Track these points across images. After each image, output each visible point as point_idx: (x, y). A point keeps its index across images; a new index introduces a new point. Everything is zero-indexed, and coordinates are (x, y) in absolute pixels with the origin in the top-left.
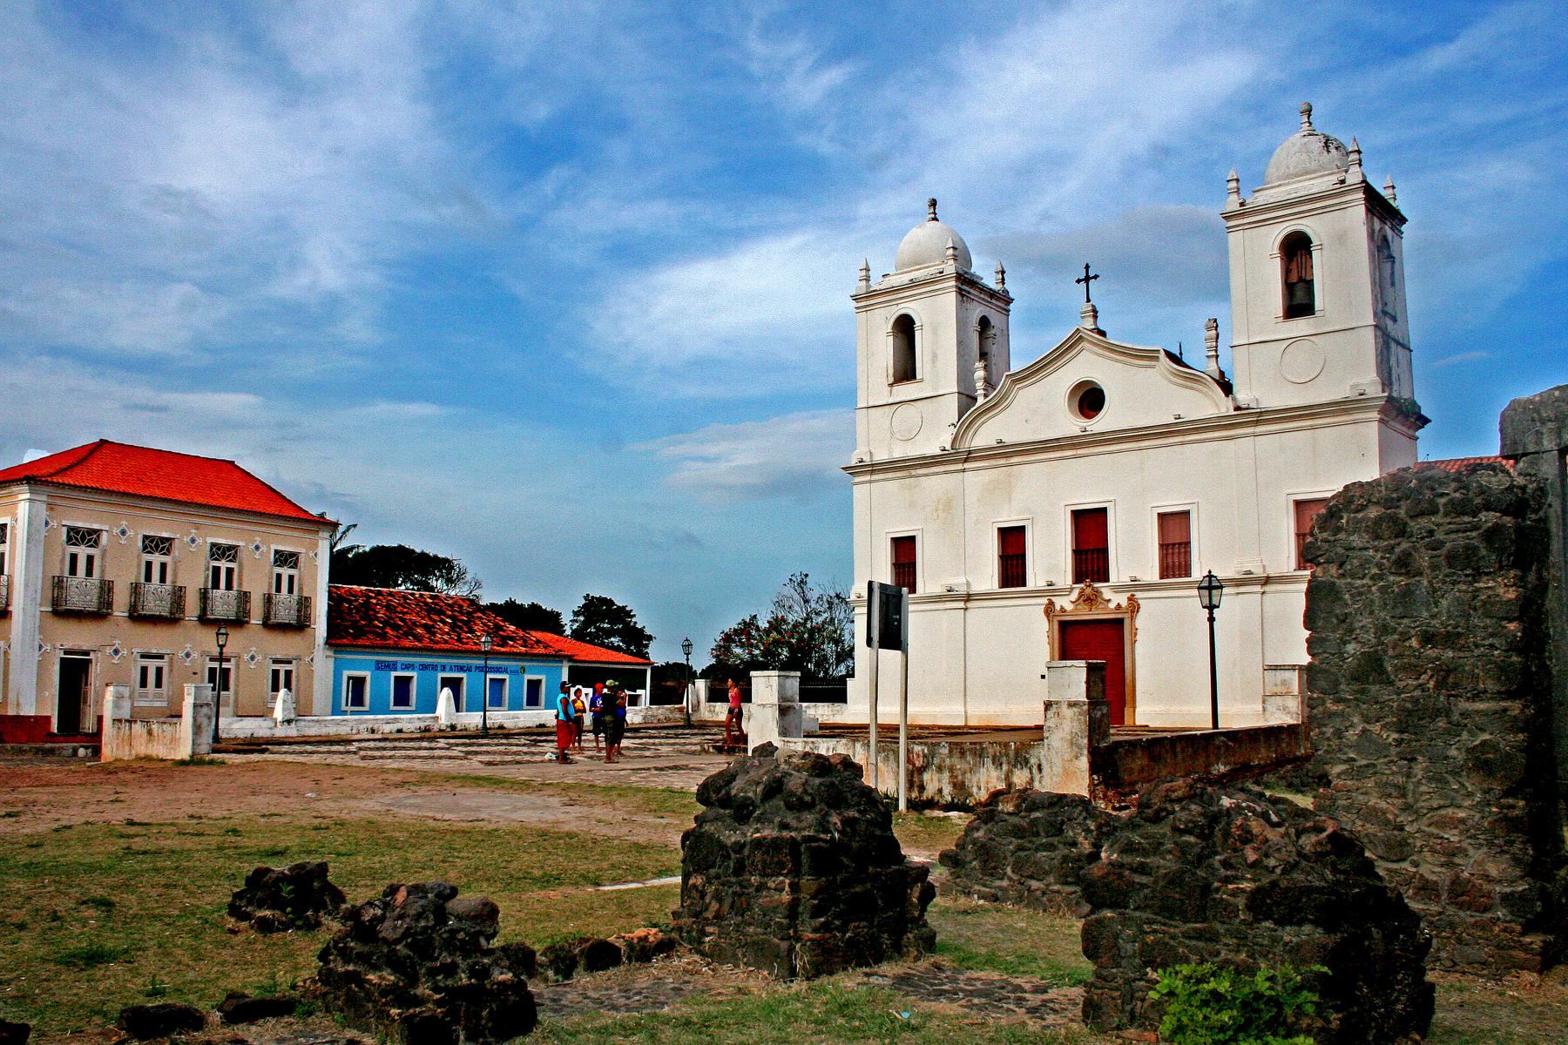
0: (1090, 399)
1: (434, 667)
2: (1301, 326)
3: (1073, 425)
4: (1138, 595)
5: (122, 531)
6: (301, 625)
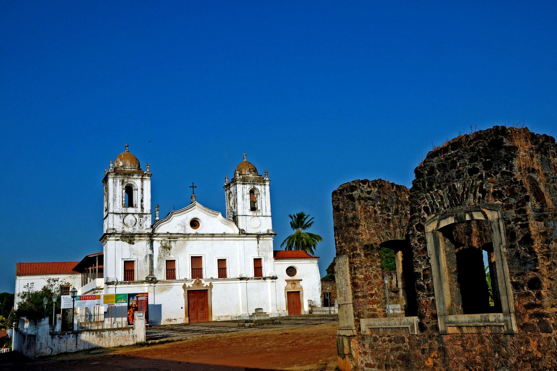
0: (194, 223)
4: (212, 282)
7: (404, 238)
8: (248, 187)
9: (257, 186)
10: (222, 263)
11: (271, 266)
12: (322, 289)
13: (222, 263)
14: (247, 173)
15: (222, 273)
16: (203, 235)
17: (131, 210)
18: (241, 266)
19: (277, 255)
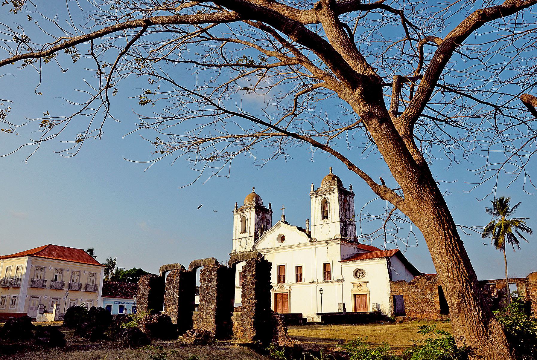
0: (282, 238)
1: (131, 303)
2: (325, 221)
3: (278, 244)
5: (51, 266)
6: (95, 290)
7: (191, 270)
8: (320, 199)
9: (326, 196)
10: (298, 269)
11: (339, 270)
12: (391, 292)
13: (298, 269)
14: (324, 185)
15: (299, 278)
16: (291, 247)
17: (244, 235)
18: (312, 272)
19: (345, 259)
